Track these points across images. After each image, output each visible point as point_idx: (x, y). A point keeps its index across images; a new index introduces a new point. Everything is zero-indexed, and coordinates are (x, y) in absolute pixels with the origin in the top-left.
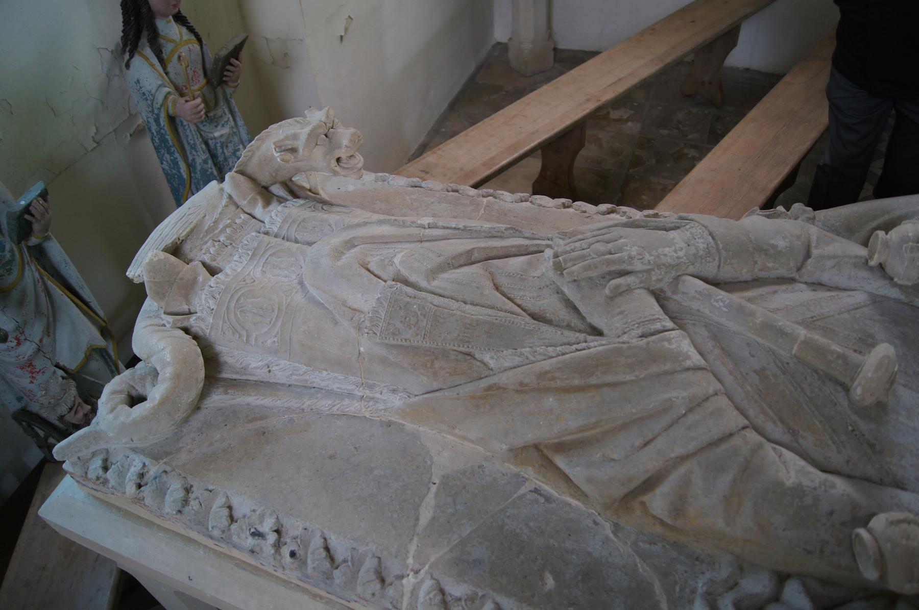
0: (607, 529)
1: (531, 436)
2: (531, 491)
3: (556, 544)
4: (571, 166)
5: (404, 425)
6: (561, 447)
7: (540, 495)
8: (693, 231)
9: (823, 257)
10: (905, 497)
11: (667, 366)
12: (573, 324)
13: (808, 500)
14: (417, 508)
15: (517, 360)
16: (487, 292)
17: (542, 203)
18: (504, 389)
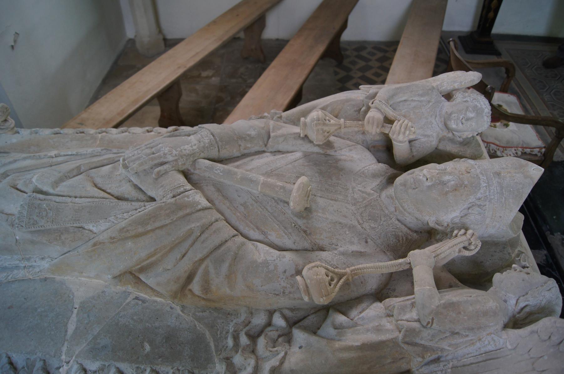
0: (178, 309)
1: (121, 266)
2: (134, 299)
3: (150, 325)
4: (177, 107)
5: (54, 278)
6: (142, 270)
7: (139, 300)
8: (202, 134)
9: (276, 137)
10: (324, 254)
11: (188, 211)
12: (139, 198)
13: (271, 267)
14: (66, 326)
15: (108, 224)
16: (89, 189)
17: (134, 131)
18: (103, 243)
